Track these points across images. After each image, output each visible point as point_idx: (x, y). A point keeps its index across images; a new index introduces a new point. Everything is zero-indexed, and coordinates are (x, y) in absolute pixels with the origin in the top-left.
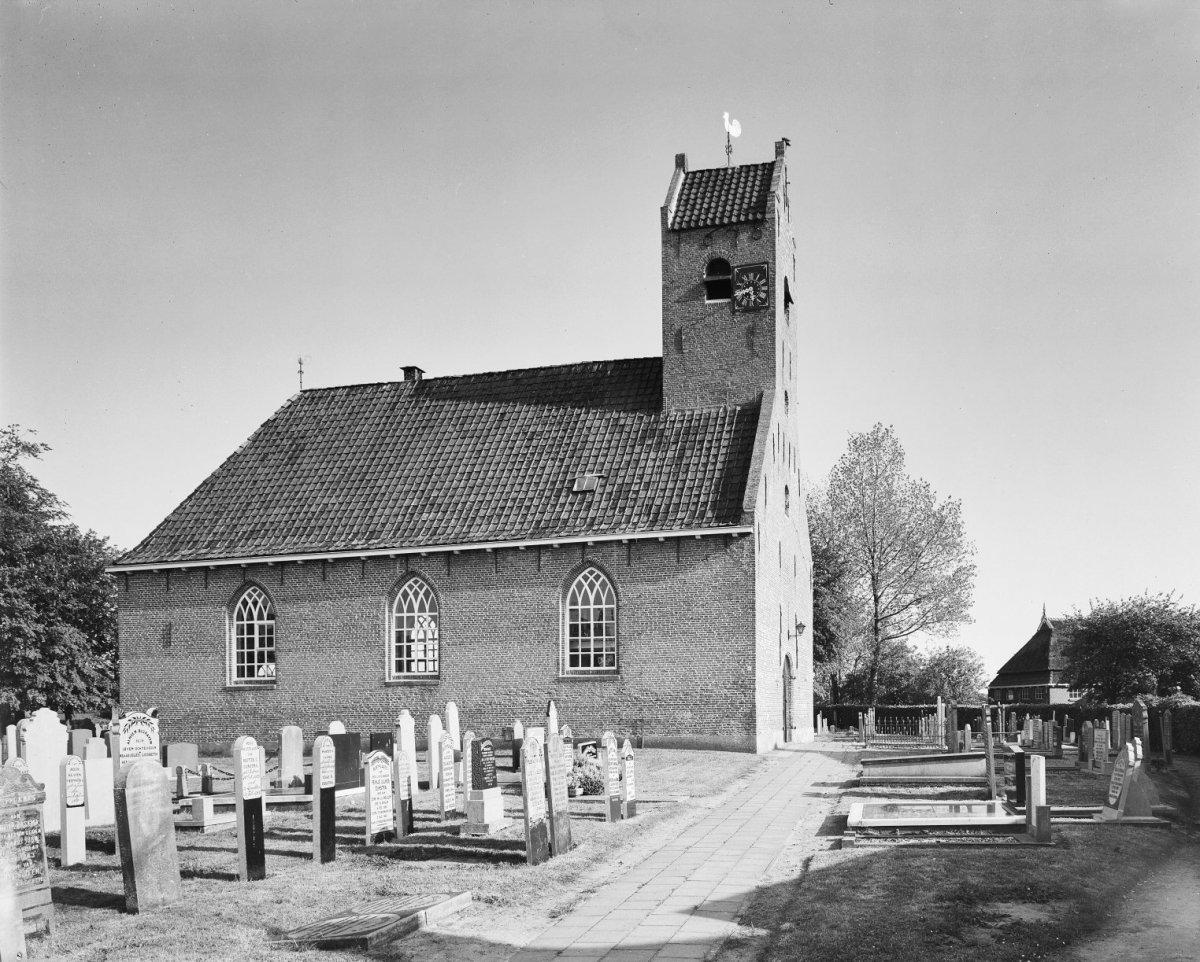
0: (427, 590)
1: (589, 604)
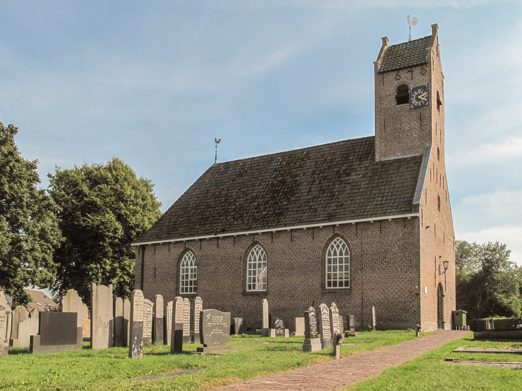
0: (262, 250)
1: (331, 256)
